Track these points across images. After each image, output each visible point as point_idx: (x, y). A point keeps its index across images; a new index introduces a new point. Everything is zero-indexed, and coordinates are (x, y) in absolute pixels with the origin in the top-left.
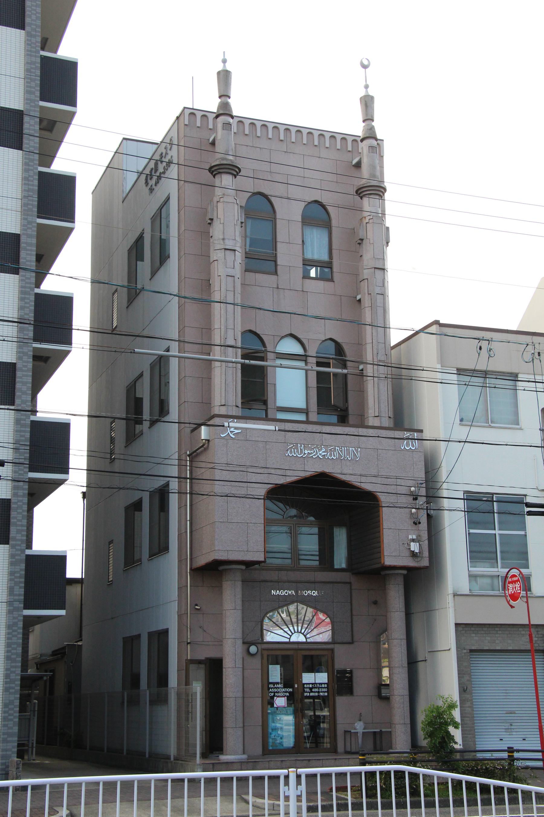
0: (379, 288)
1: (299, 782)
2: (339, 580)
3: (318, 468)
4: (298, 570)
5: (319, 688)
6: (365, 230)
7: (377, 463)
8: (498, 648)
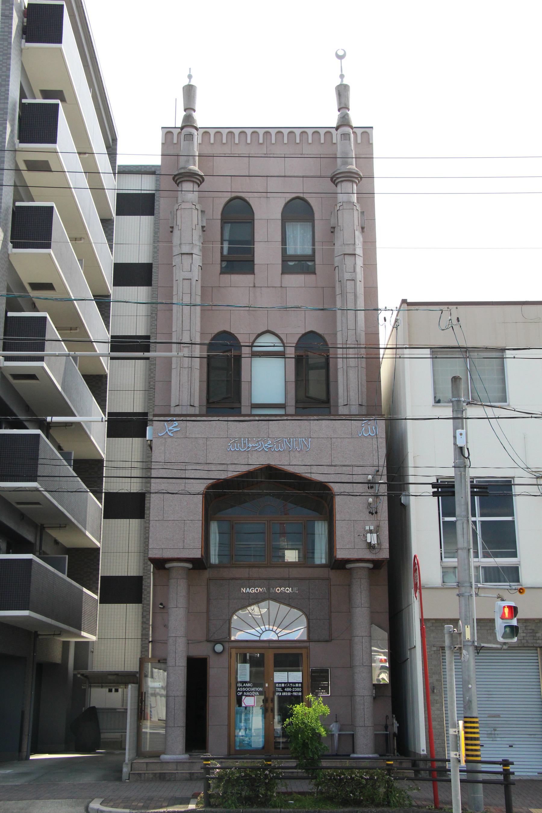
0: (350, 274)
4: (271, 567)
5: (292, 687)
6: (336, 218)
7: (330, 452)
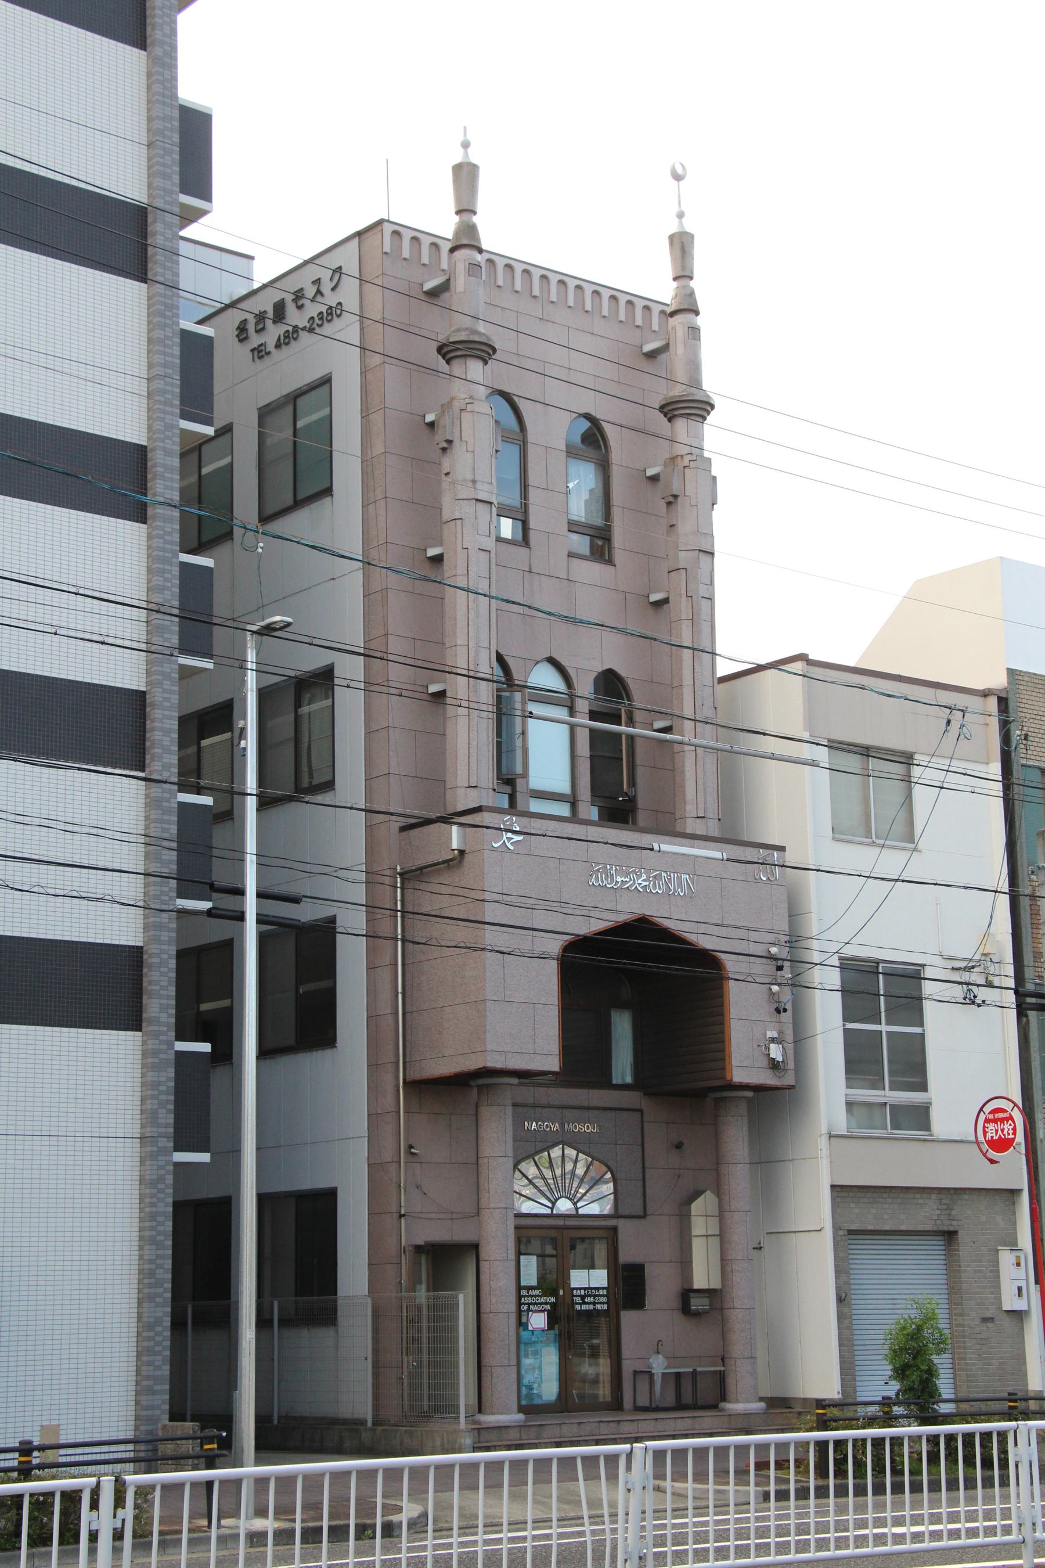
1: (119, 1501)
2: (624, 1106)
3: (626, 910)
5: (595, 1296)
8: (887, 1228)
